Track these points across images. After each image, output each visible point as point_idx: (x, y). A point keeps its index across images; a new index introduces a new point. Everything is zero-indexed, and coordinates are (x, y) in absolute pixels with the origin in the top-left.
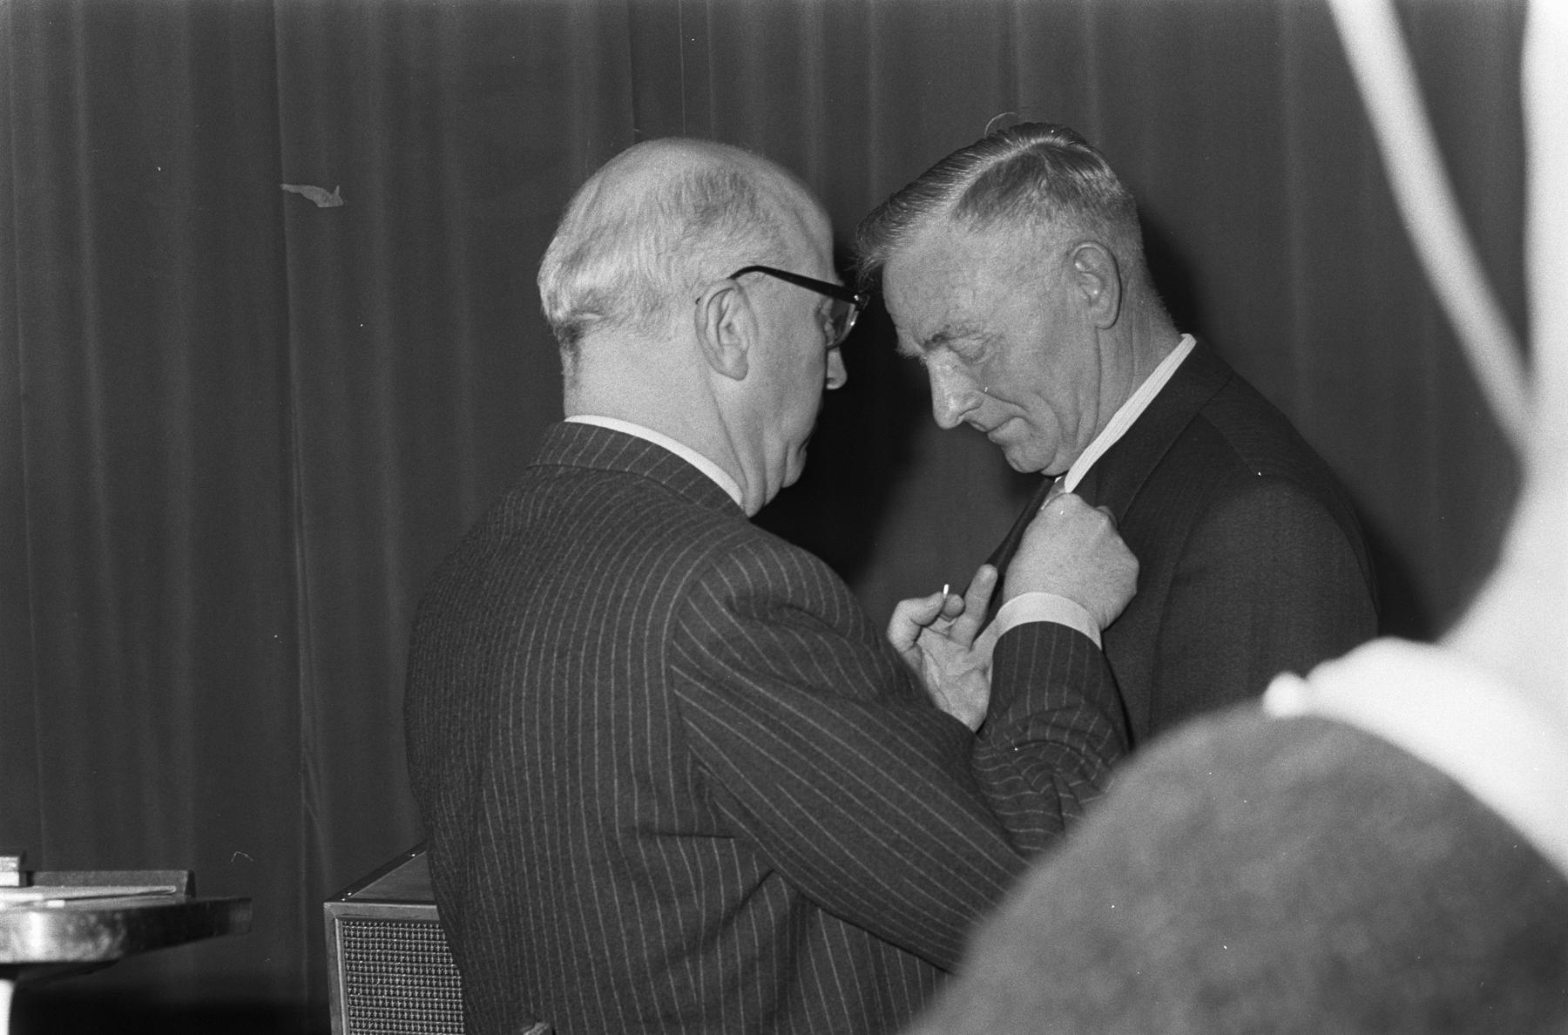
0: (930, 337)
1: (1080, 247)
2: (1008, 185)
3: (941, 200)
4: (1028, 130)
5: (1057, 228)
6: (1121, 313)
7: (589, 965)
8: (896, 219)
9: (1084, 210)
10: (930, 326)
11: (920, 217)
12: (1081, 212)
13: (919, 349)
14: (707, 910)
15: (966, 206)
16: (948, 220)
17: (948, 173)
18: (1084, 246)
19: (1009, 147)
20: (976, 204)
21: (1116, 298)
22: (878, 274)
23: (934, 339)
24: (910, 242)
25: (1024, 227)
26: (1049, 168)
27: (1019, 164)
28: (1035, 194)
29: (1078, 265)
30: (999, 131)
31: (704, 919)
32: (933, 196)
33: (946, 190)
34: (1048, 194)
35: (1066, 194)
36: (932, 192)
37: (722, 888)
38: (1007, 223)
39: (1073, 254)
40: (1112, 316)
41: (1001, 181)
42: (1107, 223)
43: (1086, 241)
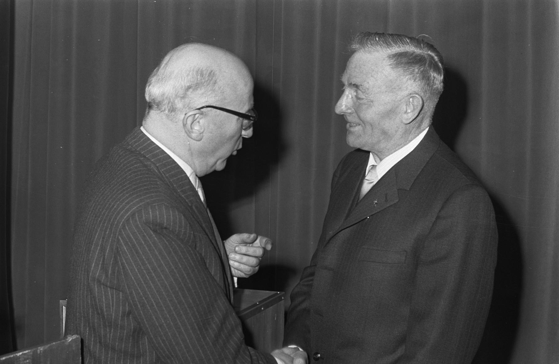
0: (353, 83)
1: (415, 95)
2: (411, 61)
3: (389, 48)
4: (431, 47)
5: (414, 85)
6: (413, 122)
7: (81, 317)
8: (372, 42)
9: (426, 85)
10: (354, 81)
11: (378, 48)
12: (425, 86)
13: (346, 83)
14: (115, 314)
15: (394, 57)
16: (386, 56)
17: (397, 41)
18: (417, 96)
19: (421, 48)
20: (398, 59)
21: (414, 118)
22: (353, 52)
23: (354, 85)
24: (370, 52)
25: (405, 78)
26: (427, 65)
27: (420, 57)
28: (417, 70)
29: (411, 99)
30: (422, 40)
31: (113, 317)
32: (387, 45)
33: (393, 46)
34: (420, 74)
35: (425, 78)
36: (388, 43)
37: (121, 308)
38: (402, 71)
39: (412, 95)
40: (408, 122)
41: (411, 58)
42: (429, 94)
43: (419, 95)
